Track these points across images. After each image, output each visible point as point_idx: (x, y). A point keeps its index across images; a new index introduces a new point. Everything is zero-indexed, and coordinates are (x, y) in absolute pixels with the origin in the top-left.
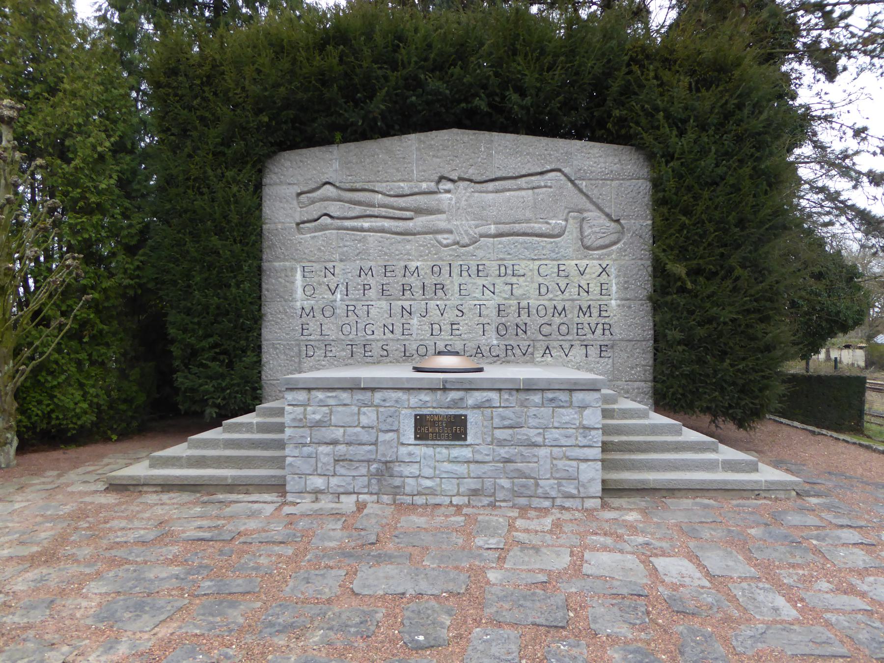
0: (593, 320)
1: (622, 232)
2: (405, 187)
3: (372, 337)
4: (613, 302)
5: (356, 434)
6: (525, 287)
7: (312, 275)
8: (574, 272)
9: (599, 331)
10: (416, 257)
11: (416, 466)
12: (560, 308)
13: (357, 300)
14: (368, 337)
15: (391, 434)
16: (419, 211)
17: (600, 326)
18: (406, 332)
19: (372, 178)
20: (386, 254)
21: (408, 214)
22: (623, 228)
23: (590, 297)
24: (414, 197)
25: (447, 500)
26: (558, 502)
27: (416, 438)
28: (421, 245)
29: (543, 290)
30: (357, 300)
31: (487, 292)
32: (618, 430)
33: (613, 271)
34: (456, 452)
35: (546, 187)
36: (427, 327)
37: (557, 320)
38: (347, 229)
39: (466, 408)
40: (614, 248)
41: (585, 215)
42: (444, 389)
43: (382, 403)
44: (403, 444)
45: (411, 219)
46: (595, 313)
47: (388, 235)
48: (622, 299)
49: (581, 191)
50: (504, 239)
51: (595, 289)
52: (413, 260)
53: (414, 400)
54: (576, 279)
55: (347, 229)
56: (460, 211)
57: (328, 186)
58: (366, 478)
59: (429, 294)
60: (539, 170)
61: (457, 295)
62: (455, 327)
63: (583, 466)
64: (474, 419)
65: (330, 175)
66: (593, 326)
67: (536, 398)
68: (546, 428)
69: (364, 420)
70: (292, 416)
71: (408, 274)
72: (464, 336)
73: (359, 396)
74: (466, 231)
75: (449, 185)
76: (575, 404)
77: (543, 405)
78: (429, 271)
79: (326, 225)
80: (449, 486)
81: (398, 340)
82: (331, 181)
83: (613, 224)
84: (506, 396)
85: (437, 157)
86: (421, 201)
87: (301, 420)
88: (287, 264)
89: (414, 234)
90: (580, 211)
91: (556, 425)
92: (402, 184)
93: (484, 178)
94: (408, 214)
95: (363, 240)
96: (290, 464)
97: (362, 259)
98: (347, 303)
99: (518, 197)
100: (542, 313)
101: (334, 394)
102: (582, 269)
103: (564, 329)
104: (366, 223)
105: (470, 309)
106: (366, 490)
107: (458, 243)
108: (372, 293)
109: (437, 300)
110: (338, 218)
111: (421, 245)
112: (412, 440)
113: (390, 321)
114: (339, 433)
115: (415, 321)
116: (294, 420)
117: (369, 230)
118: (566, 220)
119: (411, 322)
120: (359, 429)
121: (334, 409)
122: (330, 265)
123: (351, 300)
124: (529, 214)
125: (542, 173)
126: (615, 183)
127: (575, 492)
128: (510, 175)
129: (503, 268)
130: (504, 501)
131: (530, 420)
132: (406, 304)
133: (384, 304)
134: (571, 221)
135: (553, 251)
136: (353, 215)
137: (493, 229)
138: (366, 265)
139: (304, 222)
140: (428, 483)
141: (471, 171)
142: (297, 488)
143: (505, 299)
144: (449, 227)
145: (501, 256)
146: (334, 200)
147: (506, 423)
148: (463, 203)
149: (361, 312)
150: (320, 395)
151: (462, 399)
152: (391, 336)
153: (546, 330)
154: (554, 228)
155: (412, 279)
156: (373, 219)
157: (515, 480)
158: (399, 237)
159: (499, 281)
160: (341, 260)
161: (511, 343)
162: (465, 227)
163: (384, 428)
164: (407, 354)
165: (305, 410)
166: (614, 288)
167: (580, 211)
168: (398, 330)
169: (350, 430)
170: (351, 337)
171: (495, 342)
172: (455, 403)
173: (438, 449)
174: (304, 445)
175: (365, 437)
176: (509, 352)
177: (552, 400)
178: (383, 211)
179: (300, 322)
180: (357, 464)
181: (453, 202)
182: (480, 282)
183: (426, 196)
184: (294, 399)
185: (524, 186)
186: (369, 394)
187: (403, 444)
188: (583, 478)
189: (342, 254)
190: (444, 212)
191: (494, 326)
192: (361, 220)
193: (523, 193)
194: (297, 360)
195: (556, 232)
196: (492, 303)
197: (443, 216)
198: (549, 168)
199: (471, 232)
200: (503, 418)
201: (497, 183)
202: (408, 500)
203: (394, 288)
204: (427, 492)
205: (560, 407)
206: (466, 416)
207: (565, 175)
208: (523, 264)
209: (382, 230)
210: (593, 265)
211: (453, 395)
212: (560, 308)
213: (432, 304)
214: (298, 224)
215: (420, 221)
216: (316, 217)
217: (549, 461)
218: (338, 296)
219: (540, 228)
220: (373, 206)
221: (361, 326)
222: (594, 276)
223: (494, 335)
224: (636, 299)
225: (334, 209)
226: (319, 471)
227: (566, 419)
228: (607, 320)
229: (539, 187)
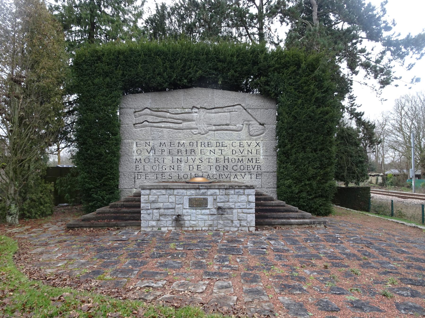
0: (254, 164)
1: (265, 130)
2: (179, 111)
3: (165, 171)
4: (261, 157)
5: (167, 205)
6: (227, 152)
7: (140, 145)
8: (246, 145)
9: (256, 168)
10: (184, 139)
11: (190, 216)
12: (241, 159)
13: (159, 156)
14: (164, 171)
15: (180, 205)
16: (184, 120)
17: (256, 166)
18: (179, 169)
19: (165, 107)
20: (171, 137)
21: (180, 121)
22: (265, 128)
23: (253, 155)
24: (182, 115)
25: (201, 229)
26: (240, 228)
27: (189, 207)
28: (185, 134)
29: (234, 152)
30: (159, 156)
31: (211, 153)
32: (262, 205)
33: (261, 144)
34: (204, 211)
35: (235, 111)
36: (188, 167)
37: (239, 164)
38: (155, 127)
39: (207, 195)
40: (262, 135)
41: (250, 122)
42: (199, 189)
43: (177, 194)
44: (184, 209)
45: (181, 123)
46: (254, 161)
47: (172, 130)
48: (265, 156)
49: (248, 113)
50: (218, 132)
51: (254, 152)
52: (182, 140)
53: (189, 192)
54: (246, 147)
55: (155, 127)
56: (201, 120)
57: (147, 109)
58: (171, 221)
59: (189, 153)
60: (232, 105)
61: (200, 154)
62: (199, 167)
63: (249, 215)
64: (210, 199)
65: (148, 105)
66: (254, 167)
67: (232, 192)
68: (235, 202)
69: (171, 200)
70: (144, 199)
71: (180, 145)
72: (203, 171)
73: (169, 191)
74: (203, 129)
75: (196, 110)
76: (246, 194)
77: (235, 194)
78: (188, 144)
79: (146, 125)
80: (201, 224)
81: (176, 172)
82: (148, 107)
83: (261, 126)
84: (222, 191)
85: (192, 99)
86: (185, 116)
87: (147, 200)
88: (130, 141)
89: (183, 130)
90: (248, 121)
91: (239, 201)
92: (177, 109)
93: (211, 107)
94: (180, 121)
95: (162, 131)
96: (143, 217)
97: (161, 139)
98: (155, 157)
99: (224, 115)
100: (234, 161)
101: (159, 191)
102: (249, 144)
103: (242, 167)
104: (163, 125)
105: (205, 160)
106: (171, 226)
107: (200, 133)
108: (165, 153)
109: (192, 156)
110: (151, 122)
111: (185, 134)
112: (188, 208)
113: (172, 164)
114: (161, 205)
115: (183, 164)
116: (145, 200)
117: (164, 128)
118: (243, 125)
119: (181, 165)
120: (168, 203)
121: (159, 196)
122: (148, 142)
123: (157, 156)
124: (228, 122)
125: (233, 106)
126: (262, 110)
127: (246, 225)
128: (221, 106)
129: (218, 143)
130: (221, 228)
131: (230, 200)
132: (179, 158)
133: (170, 158)
134: (245, 125)
135: (238, 137)
136: (158, 121)
137: (214, 128)
138: (163, 142)
139: (137, 124)
140: (194, 222)
141: (205, 105)
142: (146, 225)
143: (219, 156)
144: (196, 127)
145: (217, 139)
146: (150, 115)
147: (222, 201)
148: (202, 117)
149: (161, 161)
150: (154, 191)
151: (206, 192)
152: (173, 170)
153: (235, 168)
154: (238, 128)
155: (182, 148)
156: (166, 123)
157: (225, 221)
158: (176, 131)
159: (217, 149)
160: (152, 140)
161: (221, 173)
162: (203, 127)
163: (177, 203)
164: (180, 178)
165: (149, 197)
166: (262, 152)
167: (248, 121)
168: (176, 168)
169: (165, 204)
170: (156, 171)
171: (215, 173)
172: (203, 194)
173: (197, 210)
174: (149, 209)
175: (171, 206)
176: (221, 177)
177: (237, 192)
178: (170, 120)
179: (135, 165)
180: (168, 216)
181: (198, 117)
182: (209, 149)
183: (187, 114)
184: (145, 193)
185: (226, 111)
186: (172, 190)
187: (184, 209)
188: (249, 220)
189: (153, 137)
190: (195, 121)
191: (214, 166)
192: (161, 123)
193: (226, 114)
194: (134, 180)
195: (239, 129)
196: (213, 157)
197: (194, 122)
198: (236, 104)
199: (205, 129)
200: (220, 199)
201: (215, 110)
202: (186, 229)
203: (174, 151)
204: (193, 226)
205: (240, 195)
206: (207, 198)
207: (243, 107)
208: (226, 142)
209: (169, 128)
210: (254, 143)
211: (202, 191)
212: (241, 159)
213: (190, 158)
214: (134, 125)
215: (185, 124)
216: (142, 122)
217: (236, 214)
218: (151, 154)
219: (233, 128)
220: (166, 118)
221: (160, 166)
222: (254, 147)
223: (215, 170)
224: (270, 156)
225: (150, 119)
226: (154, 219)
227: (242, 199)
228: (259, 164)
229: (232, 111)
